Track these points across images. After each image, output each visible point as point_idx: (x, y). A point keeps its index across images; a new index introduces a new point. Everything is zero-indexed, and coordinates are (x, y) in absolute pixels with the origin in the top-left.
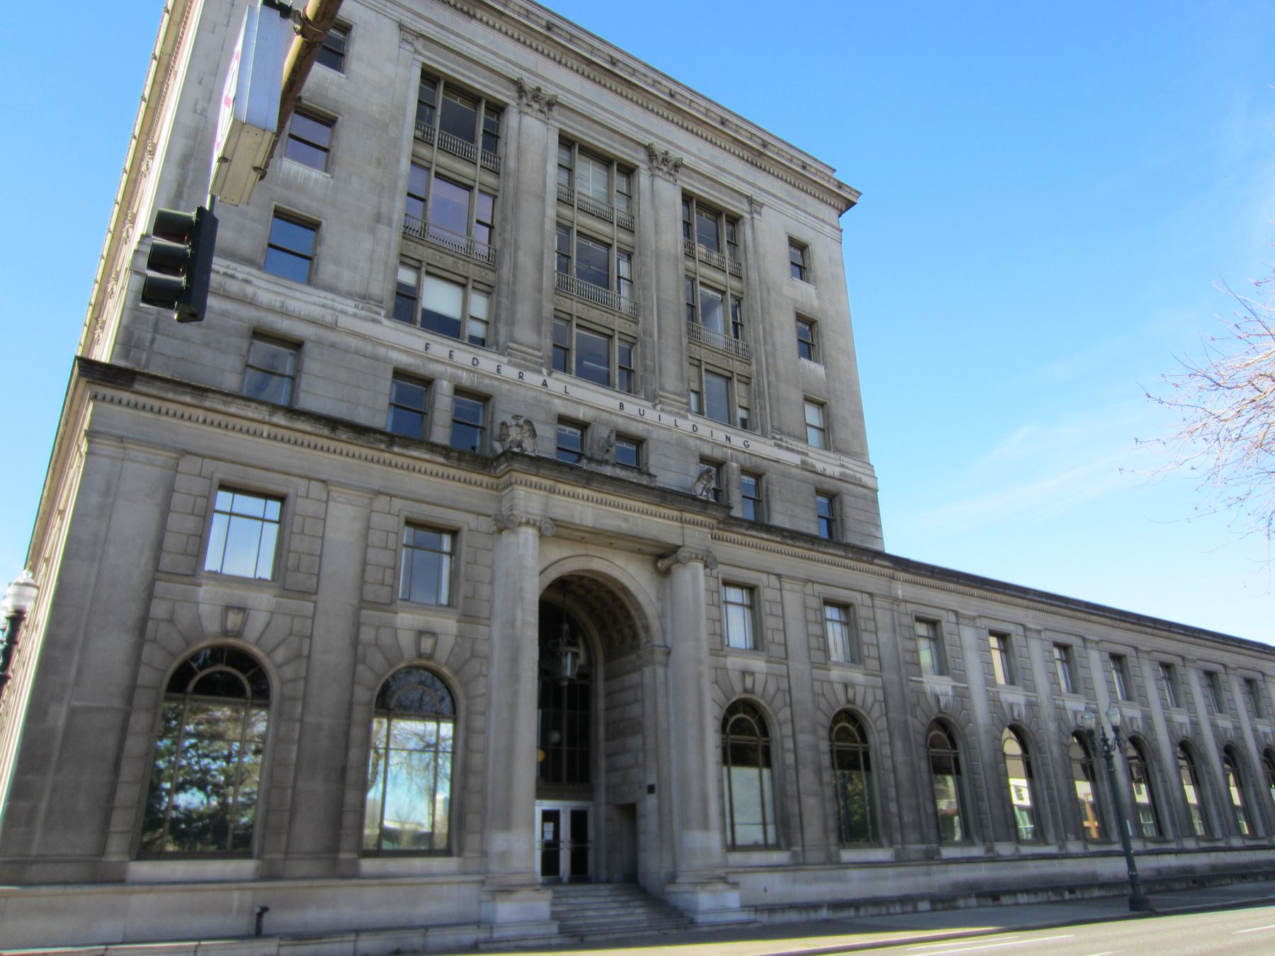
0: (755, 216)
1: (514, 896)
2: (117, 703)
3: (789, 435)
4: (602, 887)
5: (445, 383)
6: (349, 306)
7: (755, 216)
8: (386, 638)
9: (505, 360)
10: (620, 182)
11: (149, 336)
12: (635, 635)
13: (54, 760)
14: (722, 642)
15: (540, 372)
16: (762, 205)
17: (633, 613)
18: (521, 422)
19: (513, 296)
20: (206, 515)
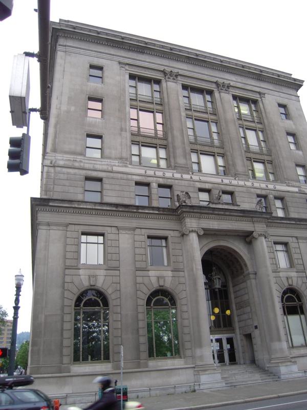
0: (263, 98)
1: (207, 373)
2: (59, 312)
3: (292, 181)
4: (242, 366)
5: (154, 184)
6: (116, 162)
7: (263, 98)
8: (76, 279)
9: (175, 171)
10: (208, 98)
11: (52, 186)
12: (242, 268)
13: (43, 332)
14: (277, 267)
15: (189, 174)
16: (264, 94)
17: (240, 260)
18: (184, 193)
19: (174, 147)
20: (78, 244)
